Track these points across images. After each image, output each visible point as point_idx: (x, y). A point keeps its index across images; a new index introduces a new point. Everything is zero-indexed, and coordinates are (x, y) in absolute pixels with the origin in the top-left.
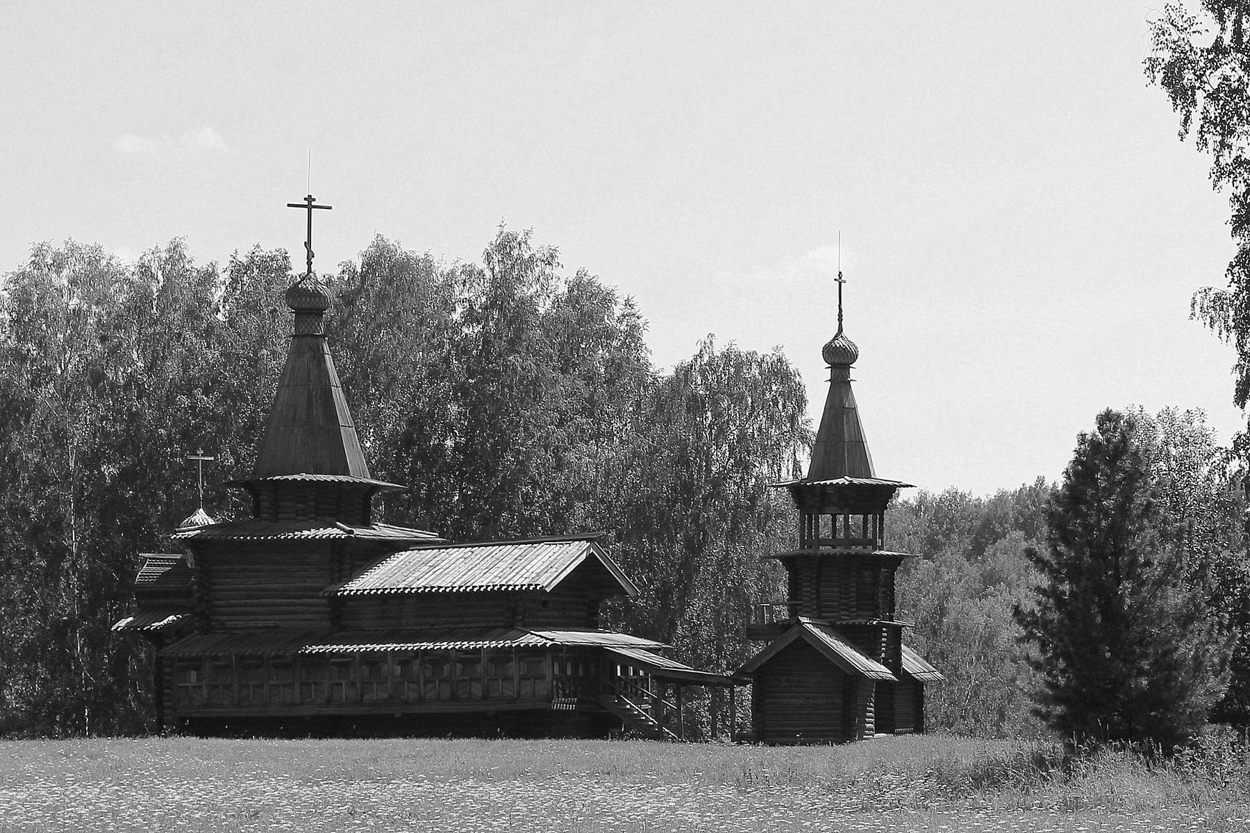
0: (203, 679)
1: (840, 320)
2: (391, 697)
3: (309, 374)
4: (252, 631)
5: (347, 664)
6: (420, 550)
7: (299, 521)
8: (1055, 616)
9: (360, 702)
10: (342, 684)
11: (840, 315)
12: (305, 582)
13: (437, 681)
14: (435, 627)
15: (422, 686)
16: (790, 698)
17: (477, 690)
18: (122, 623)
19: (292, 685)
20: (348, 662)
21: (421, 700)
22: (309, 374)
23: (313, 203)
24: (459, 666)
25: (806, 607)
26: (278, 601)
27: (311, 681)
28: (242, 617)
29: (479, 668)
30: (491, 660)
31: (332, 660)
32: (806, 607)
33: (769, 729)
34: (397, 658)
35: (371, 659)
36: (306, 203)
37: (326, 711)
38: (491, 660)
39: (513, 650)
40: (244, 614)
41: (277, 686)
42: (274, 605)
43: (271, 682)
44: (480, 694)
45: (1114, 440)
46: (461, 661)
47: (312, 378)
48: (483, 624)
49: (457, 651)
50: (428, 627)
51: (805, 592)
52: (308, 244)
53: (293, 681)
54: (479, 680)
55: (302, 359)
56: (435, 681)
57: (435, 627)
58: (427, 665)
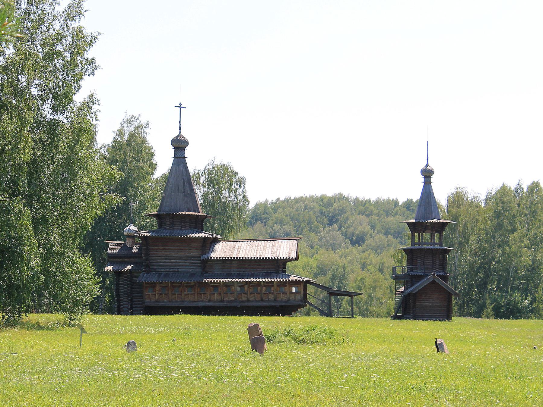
0: (156, 291)
1: (428, 159)
2: (236, 299)
4: (167, 273)
5: (217, 286)
6: (225, 242)
8: (238, 262)
9: (222, 301)
10: (228, 294)
11: (428, 158)
12: (190, 254)
13: (255, 294)
14: (245, 272)
15: (249, 296)
16: (426, 303)
17: (271, 297)
18: (129, 268)
19: (194, 294)
20: (218, 285)
21: (248, 301)
23: (182, 106)
24: (264, 288)
25: (419, 268)
27: (202, 293)
28: (164, 267)
29: (272, 289)
30: (278, 286)
31: (211, 285)
32: (419, 268)
33: (417, 314)
34: (238, 284)
36: (179, 106)
37: (274, 304)
38: (278, 286)
39: (287, 282)
40: (164, 266)
41: (188, 294)
42: (177, 262)
43: (185, 293)
44: (273, 299)
46: (265, 286)
49: (264, 282)
51: (418, 262)
52: (180, 122)
53: (194, 292)
54: (272, 293)
55: (179, 167)
56: (254, 294)
57: (245, 272)
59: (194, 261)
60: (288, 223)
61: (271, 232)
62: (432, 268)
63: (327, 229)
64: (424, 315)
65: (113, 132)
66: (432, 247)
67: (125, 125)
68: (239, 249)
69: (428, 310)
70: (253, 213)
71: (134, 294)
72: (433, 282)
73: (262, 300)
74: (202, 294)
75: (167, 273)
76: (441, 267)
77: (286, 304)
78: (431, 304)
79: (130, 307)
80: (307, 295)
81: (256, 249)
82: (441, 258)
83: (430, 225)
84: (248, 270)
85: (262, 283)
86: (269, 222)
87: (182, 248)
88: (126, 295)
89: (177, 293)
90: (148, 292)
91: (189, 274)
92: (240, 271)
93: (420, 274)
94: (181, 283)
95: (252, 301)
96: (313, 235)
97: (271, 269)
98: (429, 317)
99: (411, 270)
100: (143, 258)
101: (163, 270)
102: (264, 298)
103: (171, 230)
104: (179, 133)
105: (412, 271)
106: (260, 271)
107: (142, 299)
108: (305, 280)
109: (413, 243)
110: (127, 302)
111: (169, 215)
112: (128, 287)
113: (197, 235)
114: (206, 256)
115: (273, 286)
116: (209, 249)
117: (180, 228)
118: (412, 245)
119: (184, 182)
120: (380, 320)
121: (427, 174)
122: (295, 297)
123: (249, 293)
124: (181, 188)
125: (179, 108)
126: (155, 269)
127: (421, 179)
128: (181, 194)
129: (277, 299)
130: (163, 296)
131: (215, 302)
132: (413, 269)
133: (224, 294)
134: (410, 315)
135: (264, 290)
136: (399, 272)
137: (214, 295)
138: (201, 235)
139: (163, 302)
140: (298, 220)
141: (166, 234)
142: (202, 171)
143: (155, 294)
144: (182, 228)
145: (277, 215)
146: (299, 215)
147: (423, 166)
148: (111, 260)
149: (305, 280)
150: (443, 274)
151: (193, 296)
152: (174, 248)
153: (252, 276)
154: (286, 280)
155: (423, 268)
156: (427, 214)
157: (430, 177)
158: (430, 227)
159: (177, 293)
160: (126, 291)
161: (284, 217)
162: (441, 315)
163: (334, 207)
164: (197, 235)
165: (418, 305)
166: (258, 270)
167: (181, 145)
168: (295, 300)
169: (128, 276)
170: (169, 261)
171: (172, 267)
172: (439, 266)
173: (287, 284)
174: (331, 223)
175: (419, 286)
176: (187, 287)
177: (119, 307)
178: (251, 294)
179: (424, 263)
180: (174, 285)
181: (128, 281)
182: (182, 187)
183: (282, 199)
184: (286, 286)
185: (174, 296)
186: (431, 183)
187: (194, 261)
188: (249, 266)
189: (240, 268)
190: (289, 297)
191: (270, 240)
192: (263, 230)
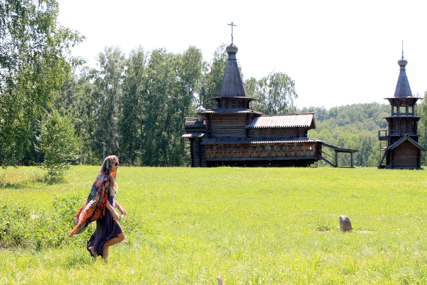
1: (403, 53)
2: (268, 156)
3: (234, 70)
4: (223, 138)
5: (255, 147)
7: (234, 109)
9: (259, 157)
11: (403, 52)
14: (276, 137)
15: (277, 153)
17: (293, 154)
18: (202, 135)
19: (239, 152)
20: (255, 146)
21: (277, 156)
22: (234, 70)
23: (233, 24)
24: (288, 147)
25: (397, 131)
26: (230, 130)
29: (294, 148)
30: (297, 146)
31: (251, 146)
32: (397, 131)
35: (262, 146)
36: (231, 24)
37: (294, 159)
38: (297, 146)
41: (235, 152)
42: (229, 131)
44: (294, 155)
45: (274, 105)
46: (288, 146)
47: (235, 71)
48: (290, 136)
50: (274, 137)
52: (232, 35)
57: (276, 137)
58: (278, 147)
59: (241, 130)
60: (347, 117)
61: (338, 122)
62: (406, 131)
63: (368, 119)
64: (400, 165)
65: (211, 53)
66: (406, 116)
67: (220, 49)
68: (272, 121)
69: (403, 162)
70: (329, 113)
71: (202, 153)
72: (407, 141)
73: (286, 156)
74: (245, 152)
75: (223, 138)
76: (413, 131)
77: (304, 158)
78: (405, 157)
79: (199, 162)
80: (322, 153)
81: (283, 121)
82: (413, 124)
83: (404, 100)
84: (278, 135)
85: (286, 144)
86: (338, 117)
87: (232, 121)
88: (197, 154)
89: (228, 152)
90: (209, 151)
91: (237, 139)
92: (272, 136)
93: (397, 135)
94: (230, 145)
95: (280, 157)
96: (360, 123)
97: (294, 135)
98: (404, 167)
99: (391, 132)
100: (207, 128)
101: (220, 136)
102: (288, 155)
103: (226, 109)
104: (231, 43)
105: (392, 134)
106: (286, 136)
107: (204, 156)
108: (316, 141)
109: (393, 114)
110: (198, 158)
111: (224, 98)
112: (198, 148)
113: (244, 112)
114: (251, 125)
115: (294, 146)
116: (252, 121)
117: (232, 107)
118: (392, 115)
119: (235, 76)
120: (137, 167)
121: (403, 64)
122: (309, 153)
123: (277, 151)
124: (233, 80)
125: (231, 26)
126: (214, 136)
127: (399, 68)
128: (233, 84)
129: (297, 155)
130: (218, 154)
131: (254, 157)
132: (393, 132)
133: (260, 152)
134: (389, 165)
135: (288, 149)
136: (383, 134)
137: (253, 153)
138: (246, 112)
139: (219, 158)
140: (352, 116)
141: (221, 111)
142: (267, 77)
143: (213, 153)
144: (233, 107)
145: (341, 113)
146: (353, 113)
147: (400, 59)
148: (187, 130)
149: (316, 141)
150: (415, 136)
151: (239, 154)
152: (227, 121)
153: (280, 139)
154: (303, 142)
155: (399, 131)
156: (403, 93)
157: (404, 66)
158: (405, 102)
159: (228, 152)
160: (197, 151)
161: (345, 114)
162: (413, 165)
163: (371, 109)
164: (244, 112)
165: (396, 158)
166: (285, 135)
167: (233, 51)
168: (309, 155)
169: (198, 141)
170: (224, 130)
171: (226, 134)
172: (412, 129)
173: (304, 145)
174: (370, 116)
175: (397, 144)
176: (234, 147)
177: (200, 162)
178: (278, 151)
179: (400, 128)
180: (226, 146)
181: (198, 144)
182: (233, 79)
183: (345, 105)
184: (303, 146)
185: (226, 154)
186: (406, 70)
187: (241, 130)
188: (278, 132)
189: (273, 134)
190: (305, 153)
191: (295, 115)
192: (334, 121)
